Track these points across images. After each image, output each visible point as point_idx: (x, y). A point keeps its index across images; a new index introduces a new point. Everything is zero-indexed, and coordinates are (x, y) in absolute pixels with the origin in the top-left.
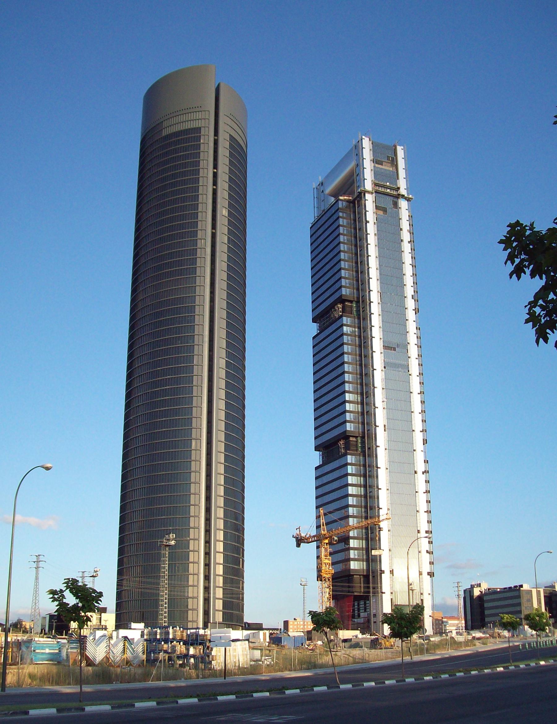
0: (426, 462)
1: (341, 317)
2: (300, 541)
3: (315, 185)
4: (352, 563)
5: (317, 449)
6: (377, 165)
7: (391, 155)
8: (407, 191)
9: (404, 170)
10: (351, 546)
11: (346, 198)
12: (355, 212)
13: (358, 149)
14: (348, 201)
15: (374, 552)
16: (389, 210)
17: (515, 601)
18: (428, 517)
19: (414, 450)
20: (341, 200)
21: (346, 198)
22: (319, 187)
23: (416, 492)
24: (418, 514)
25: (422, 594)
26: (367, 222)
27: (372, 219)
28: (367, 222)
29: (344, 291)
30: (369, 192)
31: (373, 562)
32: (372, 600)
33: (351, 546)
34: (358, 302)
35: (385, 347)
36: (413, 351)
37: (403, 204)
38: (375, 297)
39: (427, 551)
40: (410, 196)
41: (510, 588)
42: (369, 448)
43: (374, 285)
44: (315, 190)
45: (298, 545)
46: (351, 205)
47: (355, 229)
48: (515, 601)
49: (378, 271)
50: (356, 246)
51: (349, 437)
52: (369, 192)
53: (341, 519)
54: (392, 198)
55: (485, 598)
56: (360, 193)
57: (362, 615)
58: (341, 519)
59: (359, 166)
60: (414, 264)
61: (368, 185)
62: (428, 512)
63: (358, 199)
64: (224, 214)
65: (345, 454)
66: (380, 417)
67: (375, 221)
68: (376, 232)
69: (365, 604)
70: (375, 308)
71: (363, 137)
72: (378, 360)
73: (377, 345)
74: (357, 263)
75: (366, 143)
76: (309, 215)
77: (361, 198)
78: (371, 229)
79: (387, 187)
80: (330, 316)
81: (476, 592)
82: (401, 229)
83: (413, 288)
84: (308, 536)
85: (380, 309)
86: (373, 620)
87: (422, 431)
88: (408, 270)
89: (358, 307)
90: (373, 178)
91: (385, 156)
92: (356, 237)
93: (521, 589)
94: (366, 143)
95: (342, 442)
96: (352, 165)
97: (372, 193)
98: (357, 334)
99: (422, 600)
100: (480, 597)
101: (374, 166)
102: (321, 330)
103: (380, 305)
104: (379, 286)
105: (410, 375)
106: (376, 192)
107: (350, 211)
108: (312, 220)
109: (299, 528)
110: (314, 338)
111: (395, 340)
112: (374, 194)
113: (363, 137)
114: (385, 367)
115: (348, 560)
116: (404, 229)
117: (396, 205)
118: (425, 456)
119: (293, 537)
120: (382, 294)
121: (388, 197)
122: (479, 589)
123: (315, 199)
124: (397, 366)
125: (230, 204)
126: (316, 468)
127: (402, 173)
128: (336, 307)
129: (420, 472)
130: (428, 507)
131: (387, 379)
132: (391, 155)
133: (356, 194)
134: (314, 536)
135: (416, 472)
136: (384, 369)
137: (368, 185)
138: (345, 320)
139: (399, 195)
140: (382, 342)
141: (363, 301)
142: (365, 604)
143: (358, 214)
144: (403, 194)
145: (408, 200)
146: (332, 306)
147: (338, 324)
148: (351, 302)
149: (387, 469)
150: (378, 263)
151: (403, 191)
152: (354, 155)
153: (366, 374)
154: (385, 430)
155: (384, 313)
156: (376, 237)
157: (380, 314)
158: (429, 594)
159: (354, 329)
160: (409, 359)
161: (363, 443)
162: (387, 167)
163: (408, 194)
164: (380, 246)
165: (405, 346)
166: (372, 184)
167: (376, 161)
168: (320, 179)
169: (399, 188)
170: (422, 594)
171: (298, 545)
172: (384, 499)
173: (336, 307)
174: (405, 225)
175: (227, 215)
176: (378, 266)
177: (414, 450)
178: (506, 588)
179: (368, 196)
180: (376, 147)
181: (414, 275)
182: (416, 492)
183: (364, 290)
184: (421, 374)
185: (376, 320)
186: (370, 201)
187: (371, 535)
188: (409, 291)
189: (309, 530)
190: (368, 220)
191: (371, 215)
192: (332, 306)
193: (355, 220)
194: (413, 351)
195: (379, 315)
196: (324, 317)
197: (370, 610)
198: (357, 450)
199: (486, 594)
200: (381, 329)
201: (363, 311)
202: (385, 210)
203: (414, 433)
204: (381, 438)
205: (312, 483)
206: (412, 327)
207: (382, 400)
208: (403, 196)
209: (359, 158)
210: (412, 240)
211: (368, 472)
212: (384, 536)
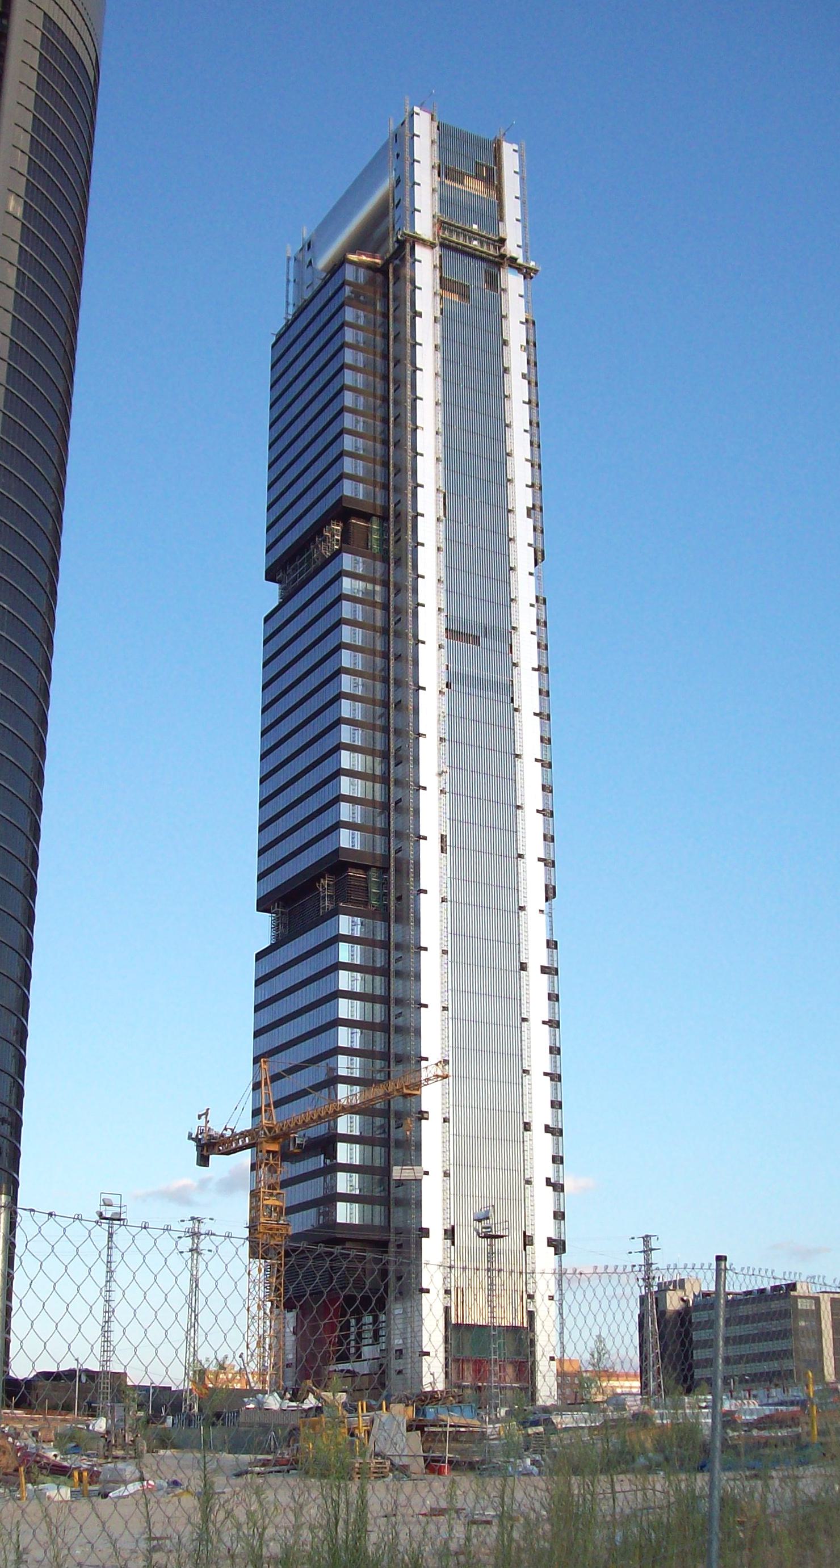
0: (552, 945)
1: (337, 554)
2: (208, 1147)
3: (291, 250)
4: (341, 1206)
5: (263, 905)
6: (447, 182)
7: (488, 161)
8: (525, 252)
9: (522, 301)
10: (339, 1160)
11: (364, 258)
12: (386, 296)
13: (401, 141)
14: (369, 267)
15: (398, 1172)
16: (475, 295)
17: (774, 1326)
18: (546, 825)
19: (522, 908)
20: (352, 262)
21: (364, 258)
22: (300, 257)
23: (524, 1020)
24: (526, 1078)
25: (531, 1297)
26: (416, 314)
27: (431, 338)
28: (416, 314)
29: (348, 488)
30: (424, 242)
31: (393, 1197)
32: (397, 1309)
33: (339, 1160)
34: (384, 518)
35: (452, 633)
36: (526, 650)
37: (513, 282)
38: (428, 502)
39: (548, 1180)
40: (532, 264)
41: (762, 1291)
42: (399, 899)
43: (428, 472)
44: (292, 263)
45: (203, 1161)
46: (379, 278)
47: (386, 336)
48: (774, 1326)
49: (441, 439)
50: (386, 378)
51: (345, 866)
52: (424, 242)
53: (318, 1087)
54: (484, 265)
55: (696, 1317)
56: (401, 244)
57: (367, 1351)
58: (318, 1087)
59: (404, 182)
60: (540, 546)
61: (424, 226)
62: (553, 1024)
63: (397, 262)
64: (11, 209)
65: (335, 913)
66: (432, 814)
67: (438, 315)
68: (439, 342)
69: (376, 1319)
70: (429, 531)
71: (416, 109)
72: (431, 665)
73: (430, 625)
74: (386, 421)
75: (423, 125)
76: (273, 309)
77: (403, 260)
78: (426, 332)
79: (472, 235)
80: (310, 556)
81: (673, 1302)
82: (505, 343)
83: (528, 435)
84: (228, 1133)
85: (442, 536)
86: (395, 1364)
87: (539, 669)
88: (519, 443)
89: (384, 531)
90: (437, 210)
91: (469, 159)
92: (386, 357)
93: (792, 1293)
94: (423, 125)
95: (325, 882)
96: (386, 185)
97: (432, 246)
98: (378, 599)
99: (531, 1315)
100: (684, 1315)
101: (441, 183)
102: (286, 599)
103: (442, 526)
104: (441, 476)
105: (516, 710)
106: (442, 245)
107: (375, 293)
108: (280, 325)
109: (206, 1114)
110: (267, 619)
111: (477, 616)
112: (437, 248)
113: (416, 109)
114: (448, 685)
115: (332, 1198)
116: (511, 343)
117: (493, 282)
118: (538, 586)
119: (190, 1137)
120: (446, 497)
121: (473, 263)
122: (680, 1293)
123: (292, 284)
124: (484, 689)
125: (30, 187)
126: (259, 956)
127: (512, 208)
128: (331, 533)
129: (534, 969)
130: (545, 803)
131: (452, 716)
132: (488, 161)
133: (391, 246)
134: (243, 1134)
135: (523, 967)
136: (445, 690)
137: (424, 226)
138: (348, 561)
139: (503, 256)
140: (443, 618)
141: (398, 515)
142: (376, 1319)
143: (394, 300)
144: (514, 255)
145: (527, 273)
146: (317, 530)
147: (329, 572)
148: (367, 517)
149: (445, 952)
150: (440, 418)
151: (513, 248)
152: (392, 155)
153: (398, 704)
154: (443, 850)
155: (452, 546)
156: (439, 355)
157: (443, 546)
158: (551, 1298)
159: (370, 586)
160: (516, 670)
161: (385, 884)
162: (474, 187)
163: (526, 259)
164: (447, 377)
165: (505, 635)
166: (434, 225)
167: (445, 171)
168: (306, 234)
169: (502, 241)
170: (531, 1297)
171: (203, 1161)
172: (433, 1038)
173: (331, 533)
174: (516, 333)
175: (19, 214)
176: (440, 426)
177: (522, 908)
178: (750, 1293)
179: (420, 252)
180: (447, 137)
181: (530, 345)
182: (524, 1020)
183: (399, 490)
184: (540, 601)
185: (429, 561)
186: (425, 268)
187: (394, 1130)
188: (521, 497)
189: (234, 1115)
190: (418, 309)
191: (426, 299)
192: (317, 530)
193: (386, 316)
194: (526, 650)
195: (439, 549)
196: (293, 563)
197: (389, 1339)
198: (366, 904)
199: (696, 1307)
200: (444, 586)
201: (396, 542)
202: (464, 292)
203: (521, 861)
204: (432, 867)
205: (245, 995)
206: (524, 587)
207: (436, 770)
208: (513, 260)
209: (403, 162)
210: (538, 503)
211: (393, 965)
212: (432, 1136)
